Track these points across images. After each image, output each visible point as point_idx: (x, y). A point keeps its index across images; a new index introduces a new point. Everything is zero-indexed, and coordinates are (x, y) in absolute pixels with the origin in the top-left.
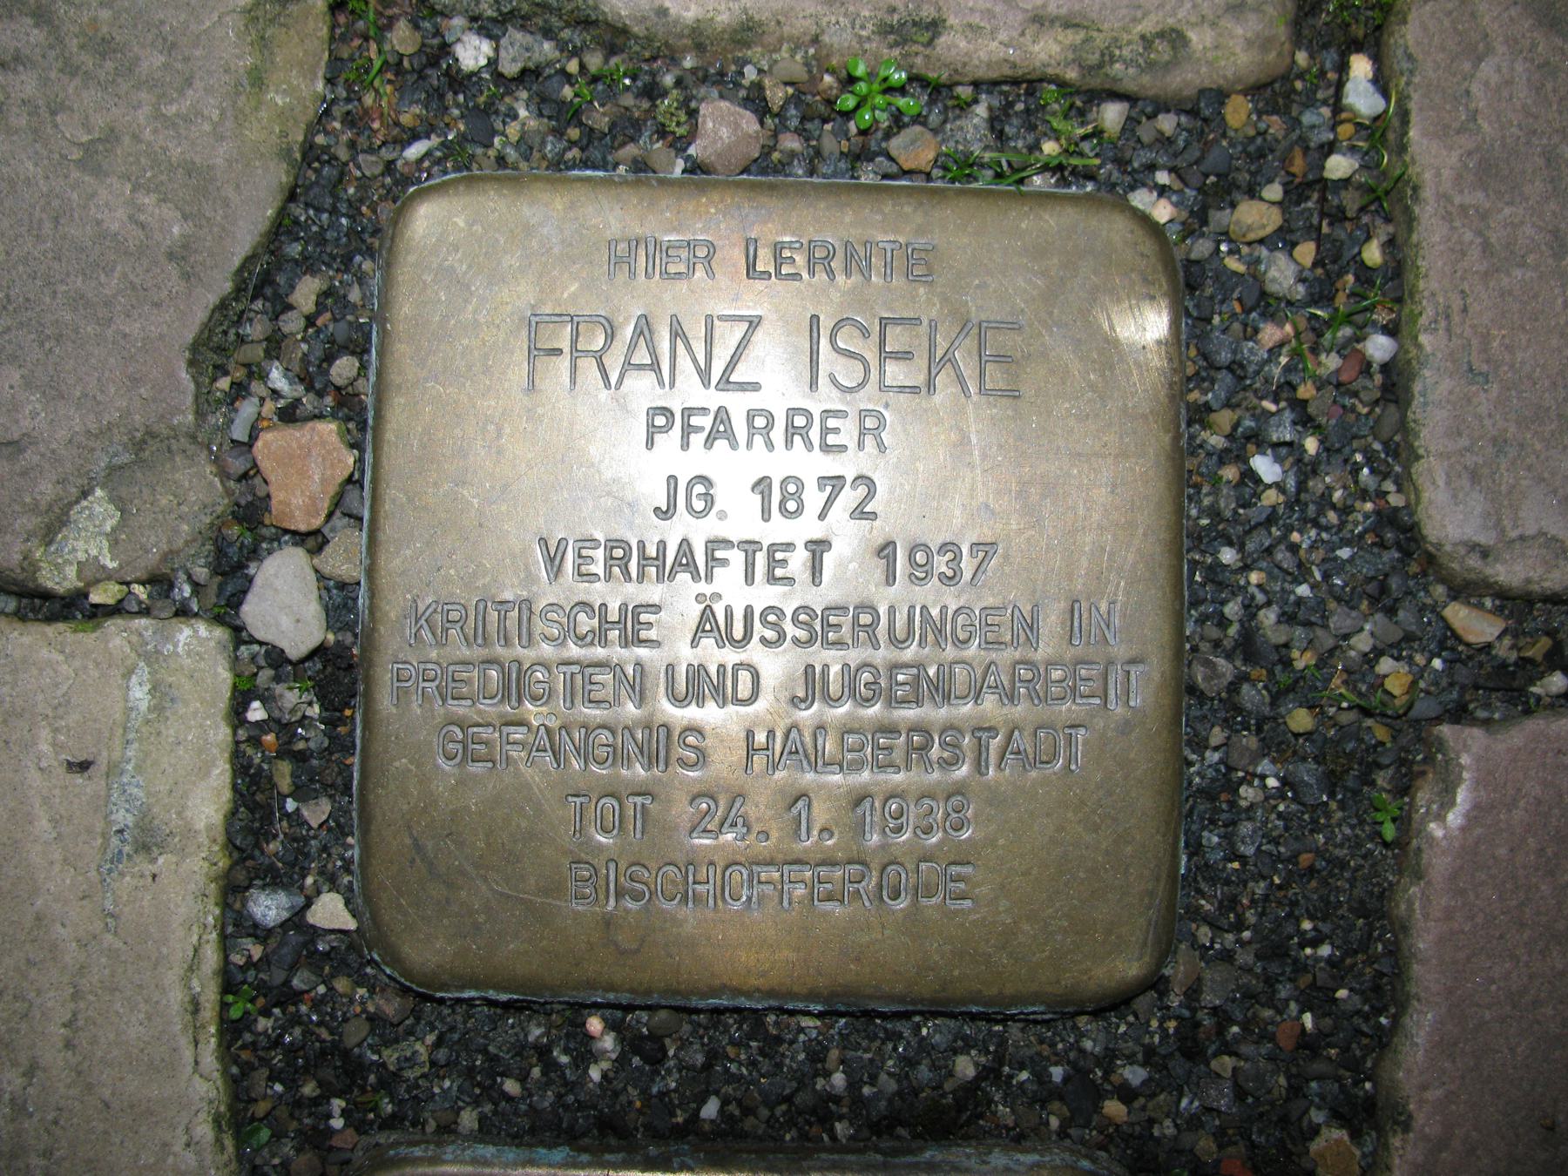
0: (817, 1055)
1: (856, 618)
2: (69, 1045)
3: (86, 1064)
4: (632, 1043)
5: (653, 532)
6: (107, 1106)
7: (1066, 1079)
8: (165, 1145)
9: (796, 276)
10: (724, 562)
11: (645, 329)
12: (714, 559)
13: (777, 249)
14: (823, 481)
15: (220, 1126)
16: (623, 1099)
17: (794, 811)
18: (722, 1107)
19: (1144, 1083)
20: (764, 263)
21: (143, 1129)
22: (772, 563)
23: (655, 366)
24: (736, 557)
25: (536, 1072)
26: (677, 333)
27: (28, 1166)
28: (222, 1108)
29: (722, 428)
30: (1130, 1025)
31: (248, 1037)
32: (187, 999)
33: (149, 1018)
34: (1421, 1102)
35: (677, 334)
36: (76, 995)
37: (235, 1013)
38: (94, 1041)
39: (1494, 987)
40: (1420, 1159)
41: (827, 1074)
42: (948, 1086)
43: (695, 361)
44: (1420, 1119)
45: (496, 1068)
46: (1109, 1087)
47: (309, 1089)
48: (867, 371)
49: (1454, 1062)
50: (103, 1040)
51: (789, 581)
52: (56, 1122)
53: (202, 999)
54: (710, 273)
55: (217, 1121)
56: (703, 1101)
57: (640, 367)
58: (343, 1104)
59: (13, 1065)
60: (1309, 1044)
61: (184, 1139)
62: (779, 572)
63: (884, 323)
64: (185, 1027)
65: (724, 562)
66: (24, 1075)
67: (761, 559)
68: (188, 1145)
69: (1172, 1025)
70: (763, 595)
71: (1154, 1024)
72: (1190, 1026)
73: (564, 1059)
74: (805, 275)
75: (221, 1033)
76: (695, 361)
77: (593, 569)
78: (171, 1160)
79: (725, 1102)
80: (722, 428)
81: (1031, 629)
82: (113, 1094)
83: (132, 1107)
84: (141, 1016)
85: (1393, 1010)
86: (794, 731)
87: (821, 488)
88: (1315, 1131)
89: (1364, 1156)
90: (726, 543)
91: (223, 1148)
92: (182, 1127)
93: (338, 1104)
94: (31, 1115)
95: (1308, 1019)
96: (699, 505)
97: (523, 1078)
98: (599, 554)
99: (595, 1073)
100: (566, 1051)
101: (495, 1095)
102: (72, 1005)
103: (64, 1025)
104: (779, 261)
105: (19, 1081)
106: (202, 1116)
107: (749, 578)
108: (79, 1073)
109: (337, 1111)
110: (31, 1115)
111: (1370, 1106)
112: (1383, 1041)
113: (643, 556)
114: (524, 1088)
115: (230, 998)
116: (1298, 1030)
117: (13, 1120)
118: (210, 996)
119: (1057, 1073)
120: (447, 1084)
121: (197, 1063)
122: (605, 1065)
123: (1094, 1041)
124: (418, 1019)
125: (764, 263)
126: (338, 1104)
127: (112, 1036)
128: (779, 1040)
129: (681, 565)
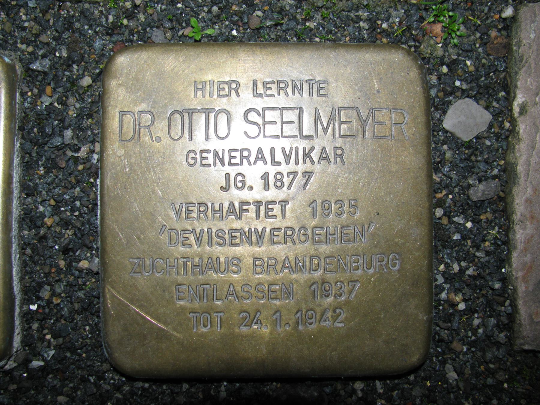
1: (285, 233)
5: (225, 199)
9: (272, 96)
10: (247, 211)
12: (268, 209)
13: (265, 84)
14: (289, 173)
17: (275, 317)
20: (261, 90)
22: (267, 210)
24: (252, 208)
29: (260, 156)
48: (260, 128)
51: (275, 217)
54: (238, 95)
62: (270, 213)
63: (264, 110)
65: (247, 211)
67: (262, 208)
70: (269, 224)
74: (276, 95)
77: (274, 213)
80: (260, 156)
81: (260, 237)
86: (231, 286)
87: (304, 176)
90: (248, 203)
96: (240, 185)
98: (195, 209)
104: (266, 88)
107: (258, 216)
113: (214, 210)
125: (261, 90)
129: (230, 212)
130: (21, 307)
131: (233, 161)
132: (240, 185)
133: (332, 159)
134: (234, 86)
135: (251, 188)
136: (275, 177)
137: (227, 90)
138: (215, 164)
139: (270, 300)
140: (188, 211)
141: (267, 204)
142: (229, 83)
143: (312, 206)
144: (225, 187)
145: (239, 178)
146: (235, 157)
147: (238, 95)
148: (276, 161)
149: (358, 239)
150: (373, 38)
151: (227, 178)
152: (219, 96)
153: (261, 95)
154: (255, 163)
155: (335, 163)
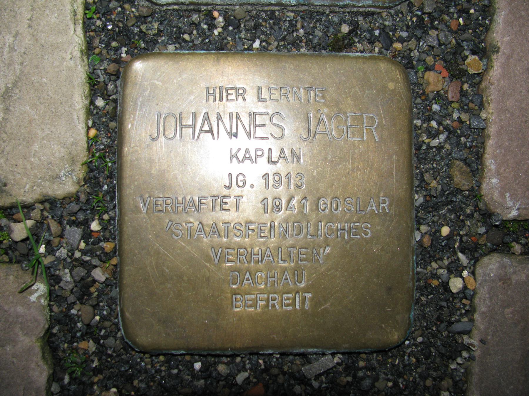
0: (293, 25)
2: (30, 26)
3: (35, 33)
4: (228, 21)
6: (43, 46)
7: (380, 34)
8: (63, 58)
11: (207, 118)
15: (82, 53)
16: (225, 41)
18: (260, 44)
19: (407, 37)
21: (55, 53)
23: (211, 131)
24: (210, 200)
25: (195, 32)
26: (219, 118)
27: (14, 68)
28: (84, 48)
29: (247, 156)
30: (400, 18)
31: (93, 28)
32: (72, 10)
33: (59, 16)
34: (502, 42)
35: (219, 119)
36: (33, 9)
37: (88, 16)
38: (39, 24)
39: (525, 4)
40: (503, 61)
41: (297, 30)
42: (339, 35)
43: (226, 129)
44: (502, 48)
45: (180, 31)
46: (395, 39)
47: (114, 44)
49: (512, 28)
50: (42, 24)
52: (24, 53)
53: (77, 12)
54: (244, 99)
55: (82, 51)
56: (254, 41)
57: (206, 132)
58: (126, 49)
59: (10, 34)
60: (462, 29)
61: (70, 56)
64: (71, 19)
66: (14, 37)
68: (71, 59)
69: (414, 19)
71: (409, 18)
72: (420, 19)
73: (205, 27)
75: (84, 23)
76: (226, 129)
78: (65, 63)
79: (262, 42)
82: (45, 42)
83: (52, 46)
84: (56, 15)
85: (490, 18)
88: (467, 57)
89: (484, 65)
91: (83, 61)
92: (69, 52)
93: (124, 49)
94: (16, 50)
95: (461, 20)
97: (190, 34)
99: (216, 32)
100: (205, 24)
101: (180, 41)
102: (31, 13)
103: (28, 20)
105: (12, 39)
106: (76, 48)
108: (33, 36)
109: (124, 52)
110: (16, 50)
111: (484, 50)
112: (488, 29)
114: (191, 37)
115: (87, 12)
116: (458, 23)
117: (9, 53)
118: (80, 10)
119: (377, 33)
120: (163, 38)
121: (75, 30)
122: (220, 30)
123: (389, 21)
124: (153, 18)
126: (124, 49)
127: (45, 23)
128: (280, 20)
130: (118, 320)
131: (230, 97)
132: (241, 184)
133: (289, 159)
134: (241, 91)
135: (252, 186)
136: (274, 178)
137: (234, 95)
138: (237, 99)
139: (246, 308)
140: (228, 94)
141: (222, 198)
142: (236, 89)
143: (263, 203)
144: (227, 185)
145: (241, 178)
146: (231, 94)
147: (244, 99)
148: (273, 160)
149: (282, 235)
150: (331, 38)
151: (230, 177)
152: (227, 100)
153: (265, 100)
154: (243, 161)
155: (292, 162)
